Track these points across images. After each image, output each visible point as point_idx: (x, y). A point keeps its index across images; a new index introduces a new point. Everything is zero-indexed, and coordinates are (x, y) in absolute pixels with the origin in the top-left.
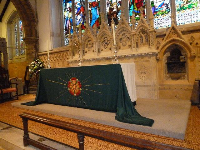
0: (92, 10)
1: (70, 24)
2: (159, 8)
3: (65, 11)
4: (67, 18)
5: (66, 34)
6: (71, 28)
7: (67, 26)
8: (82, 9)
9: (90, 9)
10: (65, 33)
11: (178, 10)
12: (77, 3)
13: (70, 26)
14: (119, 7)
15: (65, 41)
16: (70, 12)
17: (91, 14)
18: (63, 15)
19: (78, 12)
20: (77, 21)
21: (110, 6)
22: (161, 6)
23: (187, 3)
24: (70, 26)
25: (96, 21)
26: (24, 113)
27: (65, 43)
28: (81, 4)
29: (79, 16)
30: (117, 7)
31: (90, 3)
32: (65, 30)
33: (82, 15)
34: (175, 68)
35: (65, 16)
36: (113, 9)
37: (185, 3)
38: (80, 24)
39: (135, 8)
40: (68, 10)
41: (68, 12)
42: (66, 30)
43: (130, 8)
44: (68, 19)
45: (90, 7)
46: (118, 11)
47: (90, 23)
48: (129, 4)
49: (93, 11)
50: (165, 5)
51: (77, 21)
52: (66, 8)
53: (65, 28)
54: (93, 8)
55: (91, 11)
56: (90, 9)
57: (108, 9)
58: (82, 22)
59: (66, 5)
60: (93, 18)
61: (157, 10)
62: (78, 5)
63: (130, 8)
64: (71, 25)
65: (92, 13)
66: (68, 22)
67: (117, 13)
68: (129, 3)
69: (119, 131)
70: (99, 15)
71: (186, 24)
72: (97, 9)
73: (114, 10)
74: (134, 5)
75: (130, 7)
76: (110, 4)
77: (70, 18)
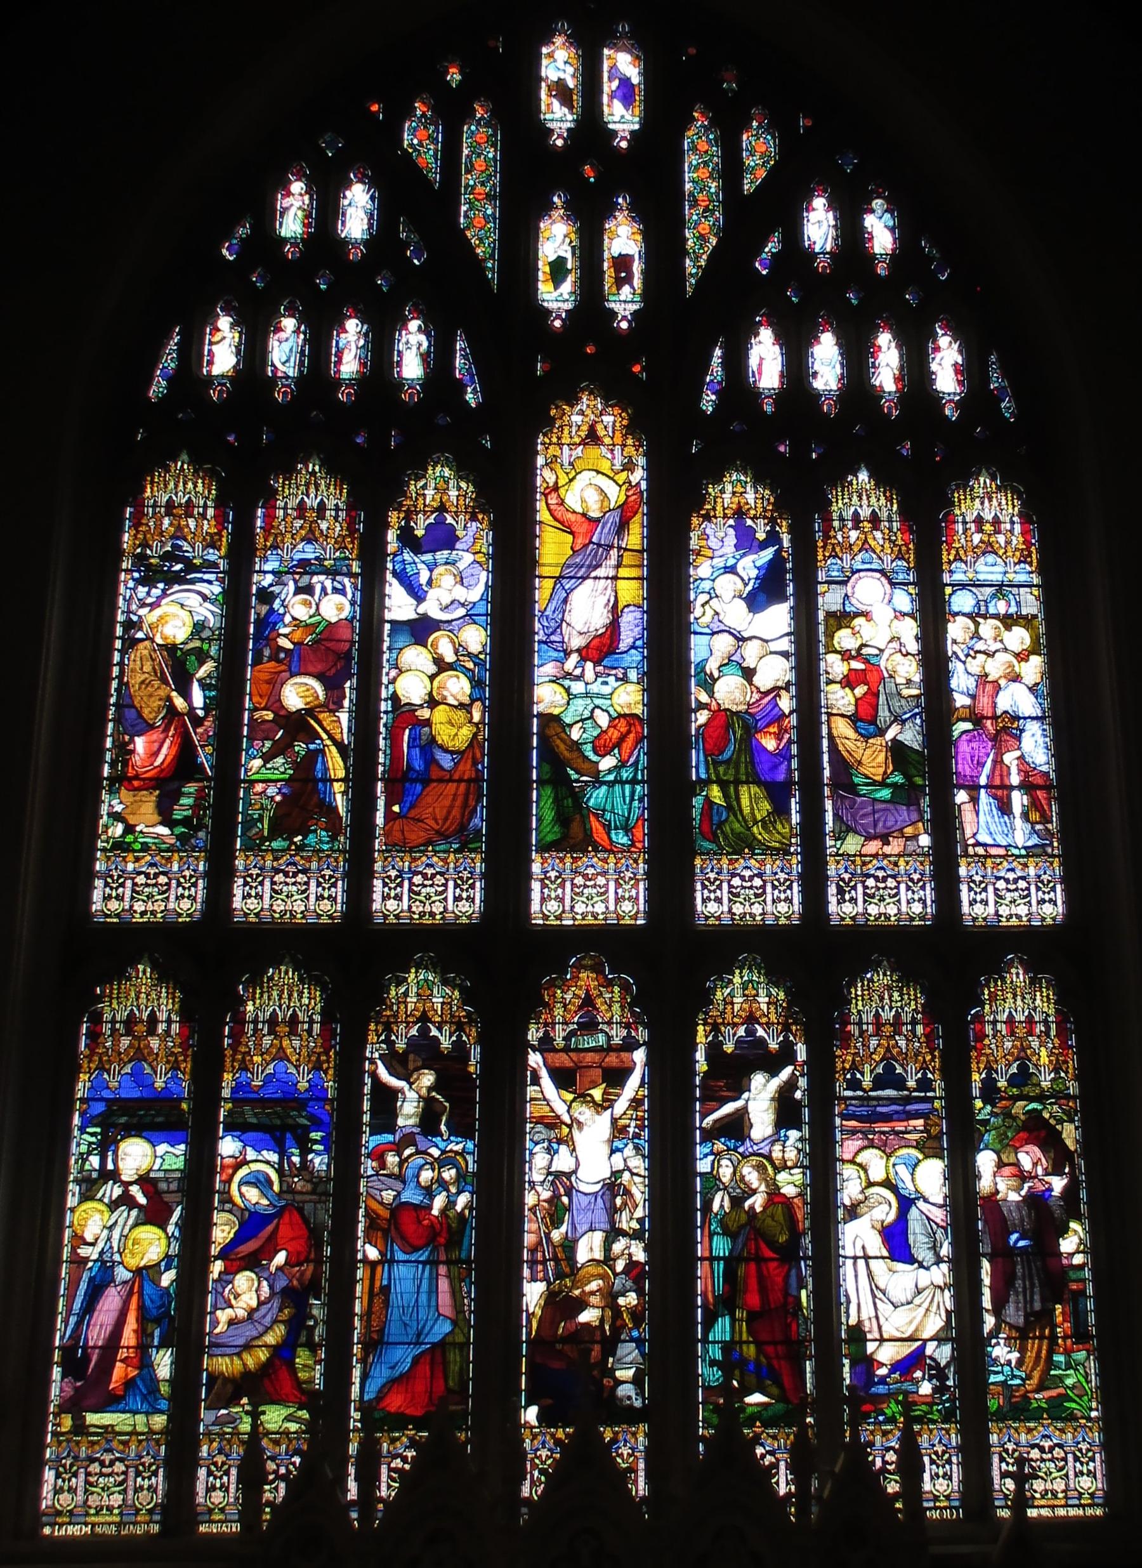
0: (387, 1260)
1: (131, 1324)
2: (897, 1375)
3: (86, 1197)
4: (106, 1268)
5: (62, 1409)
6: (145, 1363)
7: (96, 1335)
8: (285, 1231)
9: (373, 1253)
10: (55, 1390)
11: (1001, 1416)
12: (243, 1172)
13: (129, 1337)
14: (630, 1299)
15: (49, 1475)
16: (155, 1215)
17: (381, 1294)
18: (61, 1228)
19: (239, 1239)
20: (223, 1316)
21: (559, 1275)
22: (905, 1366)
23: (1040, 1388)
24: (129, 1337)
25: (416, 1361)
26: (847, 1296)
27: (47, 1489)
28: (287, 1190)
29: (244, 1280)
30: (610, 1297)
31: (375, 1205)
32: (56, 1372)
33: (281, 1283)
34: (362, 342)
35: (79, 1240)
36: (582, 1304)
37: (1034, 1381)
38: (248, 1347)
39: (741, 1342)
40: (126, 1200)
41: (125, 1217)
42: (74, 1365)
43: (706, 1333)
44: (122, 1274)
45: (369, 1240)
46: (617, 1329)
47: (363, 1361)
48: (705, 1306)
49: (402, 1272)
50: (931, 1368)
51: (223, 1316)
52: (114, 1176)
53: (68, 1351)
54: (400, 1256)
55: (382, 1274)
56: (373, 1253)
57: (533, 1293)
58: (270, 1339)
59: (107, 1145)
60: (394, 1331)
61: (881, 1389)
62: (243, 1183)
63: (706, 1333)
64: (142, 1333)
65: (386, 1290)
66: (111, 1301)
67: (610, 1345)
68: (704, 1294)
69: (997, 578)
70: (454, 1323)
71: (137, 919)
72: (443, 1269)
73: (588, 1316)
74: (733, 1320)
75: (709, 1324)
76: (555, 1259)
77: (139, 1272)
